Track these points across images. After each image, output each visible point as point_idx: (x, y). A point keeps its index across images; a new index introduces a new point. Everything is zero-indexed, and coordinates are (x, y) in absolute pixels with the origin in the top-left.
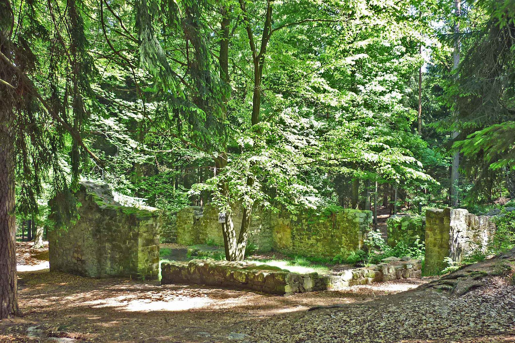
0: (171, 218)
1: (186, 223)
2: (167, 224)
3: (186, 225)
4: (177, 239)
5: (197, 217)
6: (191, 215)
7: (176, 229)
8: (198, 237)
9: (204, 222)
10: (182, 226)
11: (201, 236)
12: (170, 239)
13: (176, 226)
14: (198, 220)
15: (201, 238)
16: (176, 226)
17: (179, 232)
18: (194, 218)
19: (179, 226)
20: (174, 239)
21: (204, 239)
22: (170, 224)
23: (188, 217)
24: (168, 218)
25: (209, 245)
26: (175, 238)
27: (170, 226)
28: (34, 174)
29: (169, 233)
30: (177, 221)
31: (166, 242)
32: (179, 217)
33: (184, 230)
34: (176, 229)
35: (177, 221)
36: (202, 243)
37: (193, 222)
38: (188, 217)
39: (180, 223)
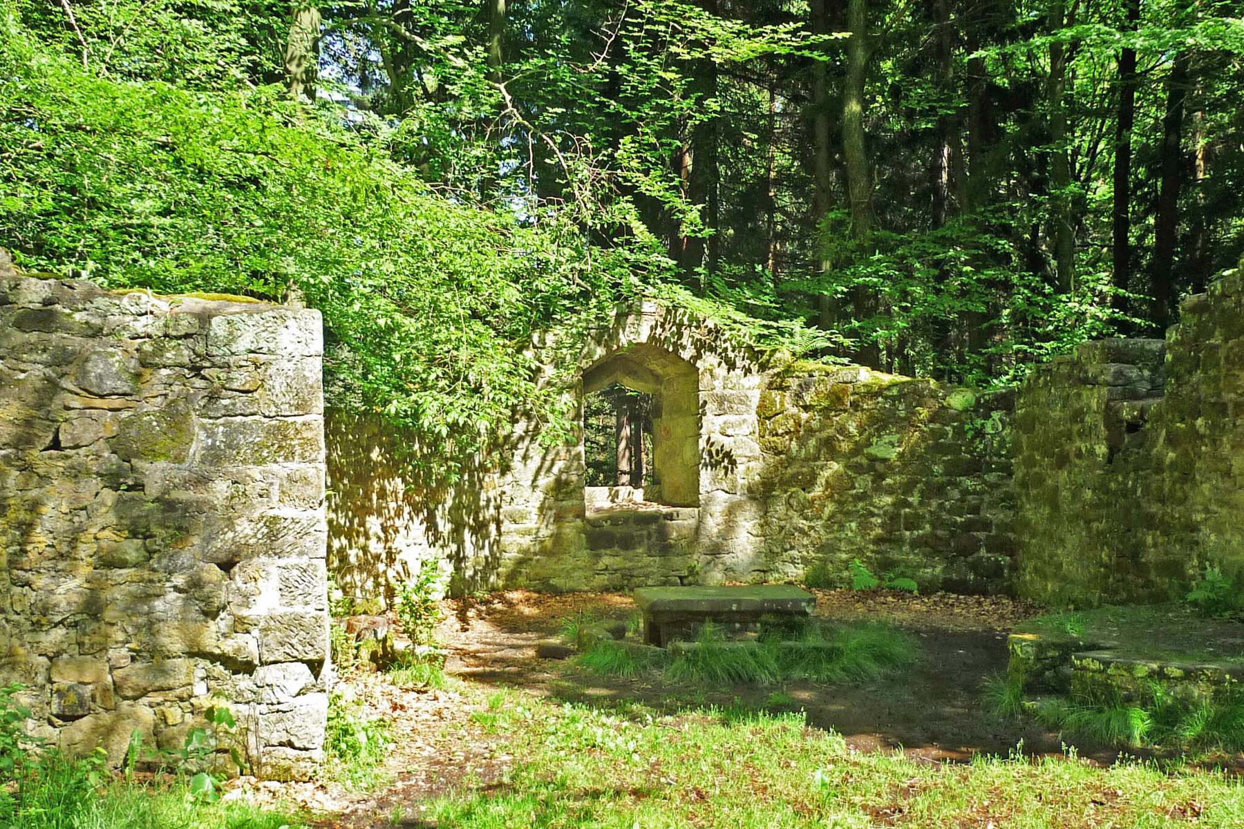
0: (980, 433)
1: (1062, 461)
2: (957, 469)
3: (1063, 475)
4: (1014, 568)
5: (1127, 411)
6: (1093, 399)
7: (1010, 502)
8: (1136, 552)
9: (1172, 441)
10: (1040, 480)
11: (1153, 546)
12: (974, 567)
13: (1012, 485)
14: (1133, 427)
15: (1151, 556)
16: (1012, 485)
17: (1027, 524)
18: (1110, 415)
19: (1024, 484)
20: (997, 571)
21: (1173, 568)
22: (975, 467)
23: (1078, 416)
24: (959, 432)
25: (1208, 609)
26: (1004, 560)
27: (968, 483)
28: (60, 632)
29: (968, 526)
30: (1015, 450)
31: (950, 586)
32: (1026, 425)
33: (1055, 506)
34: (1010, 502)
35: (1015, 450)
36: (1158, 599)
37: (1101, 449)
38: (1078, 416)
39: (1030, 462)
